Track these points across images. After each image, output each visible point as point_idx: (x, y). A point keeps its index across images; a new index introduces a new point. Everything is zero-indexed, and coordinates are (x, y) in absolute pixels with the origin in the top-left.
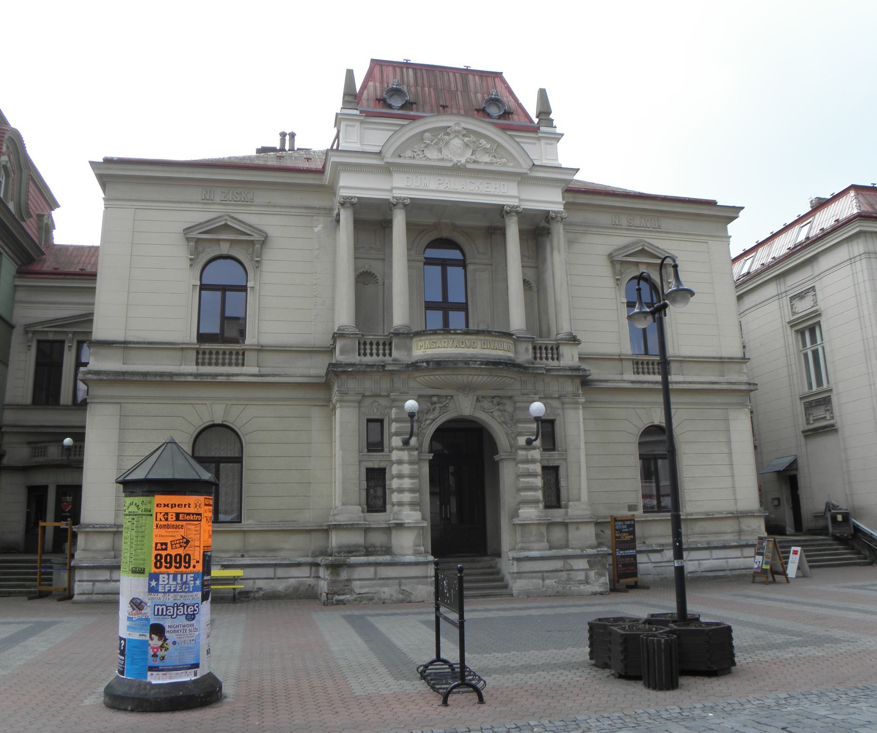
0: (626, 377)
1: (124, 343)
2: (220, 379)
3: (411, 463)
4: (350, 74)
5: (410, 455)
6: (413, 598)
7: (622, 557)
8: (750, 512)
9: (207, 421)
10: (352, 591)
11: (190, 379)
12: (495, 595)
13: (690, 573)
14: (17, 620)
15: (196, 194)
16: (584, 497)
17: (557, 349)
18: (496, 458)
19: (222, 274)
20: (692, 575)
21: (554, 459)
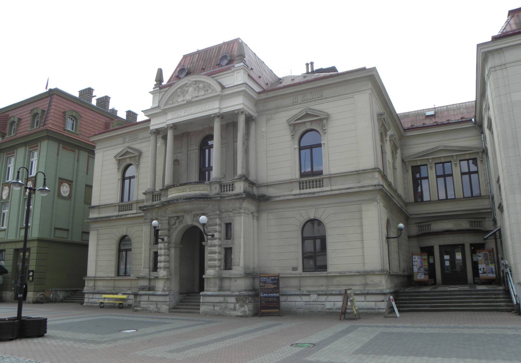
0: (294, 192)
1: (99, 206)
2: (316, 195)
4: (160, 72)
5: (164, 245)
6: (161, 311)
7: (265, 297)
8: (372, 271)
9: (306, 218)
10: (140, 307)
11: (114, 218)
12: (193, 313)
13: (328, 309)
14: (391, 325)
15: (120, 140)
16: (242, 264)
17: (233, 185)
18: (203, 243)
19: (307, 140)
20: (329, 310)
21: (228, 243)
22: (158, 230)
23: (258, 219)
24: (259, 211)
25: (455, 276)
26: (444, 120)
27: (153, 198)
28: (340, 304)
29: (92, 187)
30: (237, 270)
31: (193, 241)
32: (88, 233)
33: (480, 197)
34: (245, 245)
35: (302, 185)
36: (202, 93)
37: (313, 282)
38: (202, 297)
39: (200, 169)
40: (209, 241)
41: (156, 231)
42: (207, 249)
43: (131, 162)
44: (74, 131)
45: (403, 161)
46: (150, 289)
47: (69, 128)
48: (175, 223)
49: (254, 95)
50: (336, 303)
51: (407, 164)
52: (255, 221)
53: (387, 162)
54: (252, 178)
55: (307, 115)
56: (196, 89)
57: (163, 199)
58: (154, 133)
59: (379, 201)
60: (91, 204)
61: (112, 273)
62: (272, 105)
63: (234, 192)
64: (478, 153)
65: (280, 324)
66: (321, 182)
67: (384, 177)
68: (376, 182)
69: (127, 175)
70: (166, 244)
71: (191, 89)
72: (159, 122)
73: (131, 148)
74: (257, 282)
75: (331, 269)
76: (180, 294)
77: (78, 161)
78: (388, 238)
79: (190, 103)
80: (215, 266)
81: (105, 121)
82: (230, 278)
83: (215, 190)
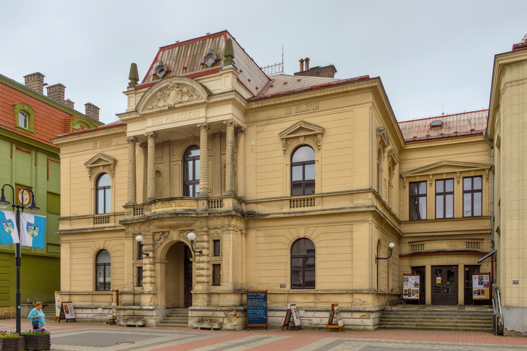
3: (150, 264)
4: (134, 68)
8: (360, 290)
15: (90, 145)
16: (230, 280)
17: (221, 201)
18: (191, 260)
22: (143, 245)
23: (246, 235)
24: (247, 228)
25: (444, 296)
26: (451, 132)
27: (134, 212)
28: (326, 321)
29: (59, 195)
30: (227, 285)
31: (180, 257)
32: (59, 245)
33: (481, 217)
34: (233, 262)
35: (292, 202)
36: (186, 98)
37: (301, 300)
38: (190, 312)
39: (184, 182)
40: (197, 258)
41: (140, 245)
42: (195, 266)
43: (105, 171)
44: (27, 129)
45: (401, 177)
46: (134, 304)
47: (21, 124)
48: (160, 238)
49: (243, 104)
50: (323, 319)
51: (405, 179)
52: (244, 238)
53: (383, 181)
54: (240, 194)
55: (301, 129)
56: (178, 93)
57: (147, 213)
58: (132, 141)
59: (371, 222)
60: (60, 214)
61: (90, 288)
62: (263, 115)
63: (223, 209)
64: (484, 170)
65: (270, 337)
66: (313, 201)
67: (378, 197)
68: (369, 203)
69: (101, 184)
70: (151, 260)
71: (173, 93)
72: (139, 128)
73: (104, 156)
74: (245, 297)
75: (320, 285)
76: (166, 308)
77: (35, 165)
78: (377, 259)
79: (172, 109)
80: (203, 282)
81: (64, 118)
82: (219, 294)
83: (202, 205)
